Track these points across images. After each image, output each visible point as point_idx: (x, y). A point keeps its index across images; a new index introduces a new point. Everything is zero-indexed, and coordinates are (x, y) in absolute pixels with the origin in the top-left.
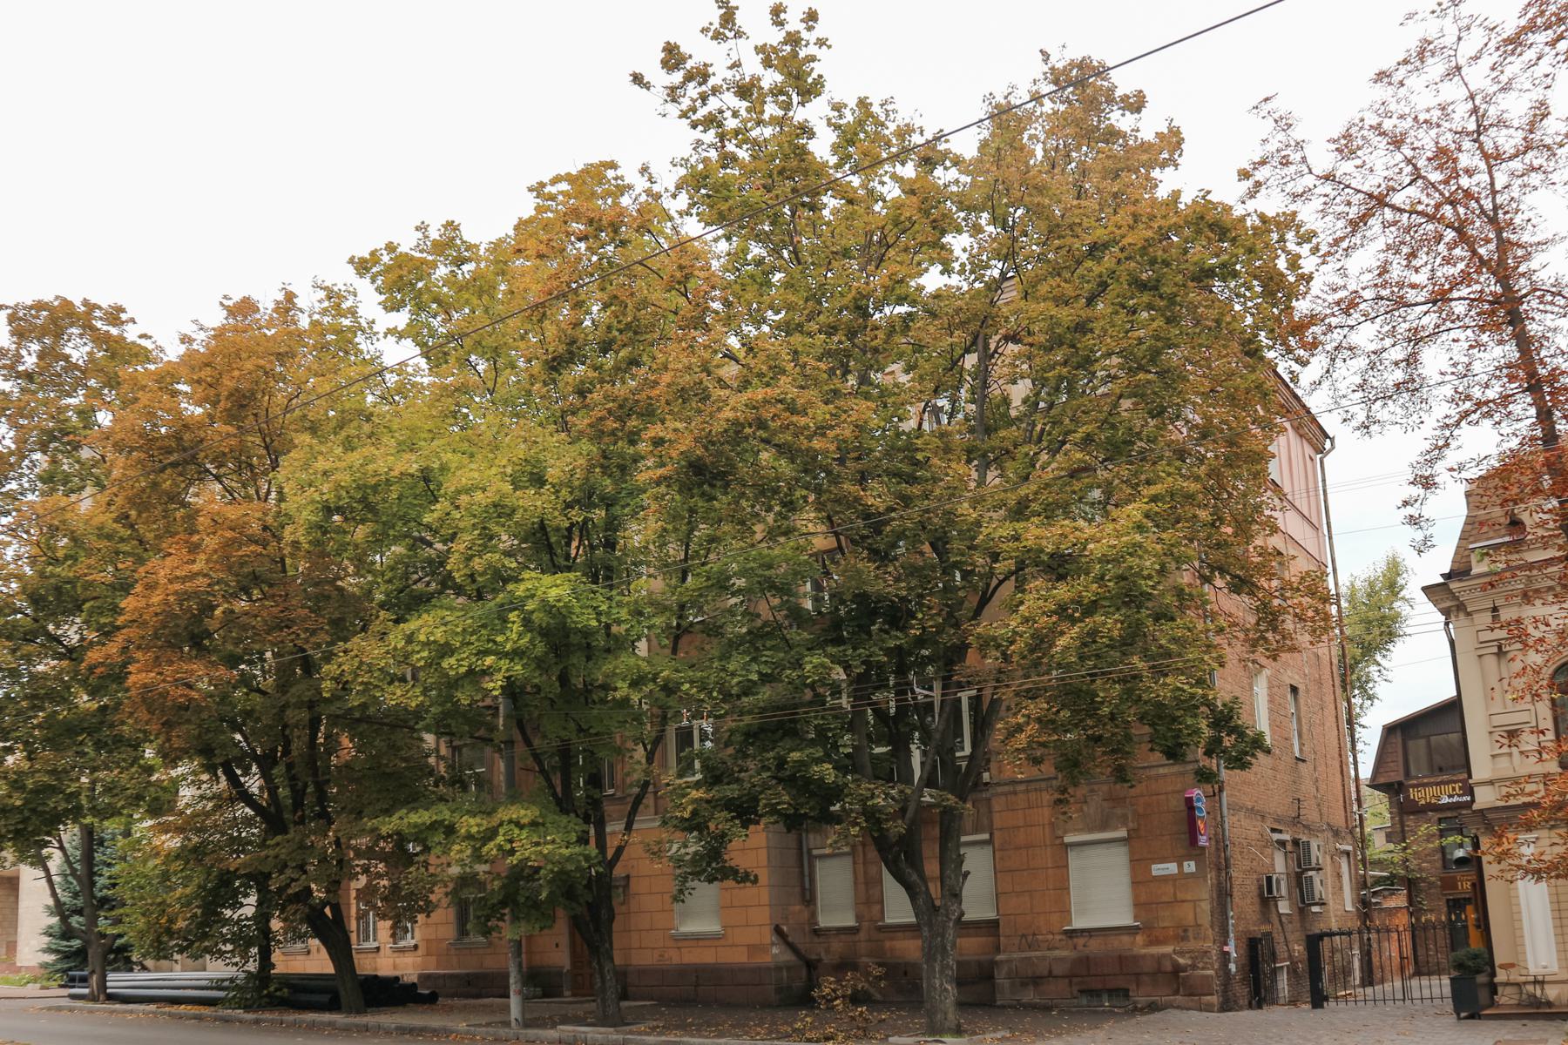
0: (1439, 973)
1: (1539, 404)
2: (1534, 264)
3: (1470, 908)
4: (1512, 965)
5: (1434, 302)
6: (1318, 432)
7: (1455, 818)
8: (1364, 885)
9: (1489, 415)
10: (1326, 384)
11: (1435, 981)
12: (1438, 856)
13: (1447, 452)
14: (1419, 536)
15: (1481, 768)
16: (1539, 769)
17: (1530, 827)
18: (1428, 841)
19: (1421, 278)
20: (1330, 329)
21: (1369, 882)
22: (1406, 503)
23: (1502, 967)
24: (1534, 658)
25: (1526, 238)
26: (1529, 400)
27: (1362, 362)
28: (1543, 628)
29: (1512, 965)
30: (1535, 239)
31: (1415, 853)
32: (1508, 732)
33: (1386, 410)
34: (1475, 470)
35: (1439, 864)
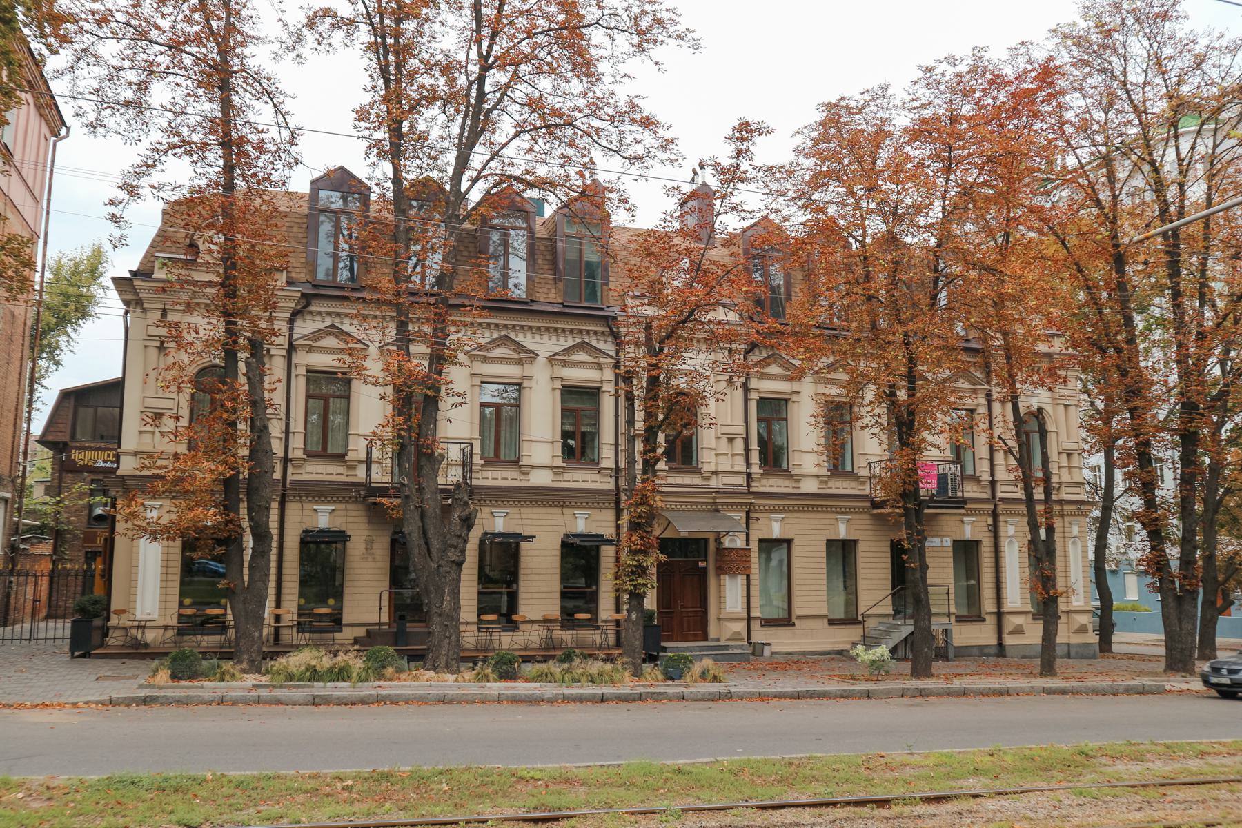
0: (64, 617)
1: (227, 157)
2: (247, 51)
3: (99, 559)
4: (124, 612)
5: (171, 48)
6: (57, 118)
7: (105, 481)
8: (16, 533)
9: (189, 153)
10: (67, 77)
11: (60, 624)
12: (85, 512)
13: (152, 171)
14: (118, 233)
15: (130, 439)
16: (171, 448)
17: (155, 495)
18: (79, 498)
19: (165, 24)
20: (81, 31)
21: (21, 528)
22: (112, 203)
23: (116, 612)
24: (185, 358)
25: (246, 29)
26: (220, 152)
27: (103, 72)
28: (193, 334)
29: (124, 612)
30: (252, 33)
31: (67, 507)
32: (155, 414)
33: (113, 119)
34: (170, 193)
35: (85, 520)
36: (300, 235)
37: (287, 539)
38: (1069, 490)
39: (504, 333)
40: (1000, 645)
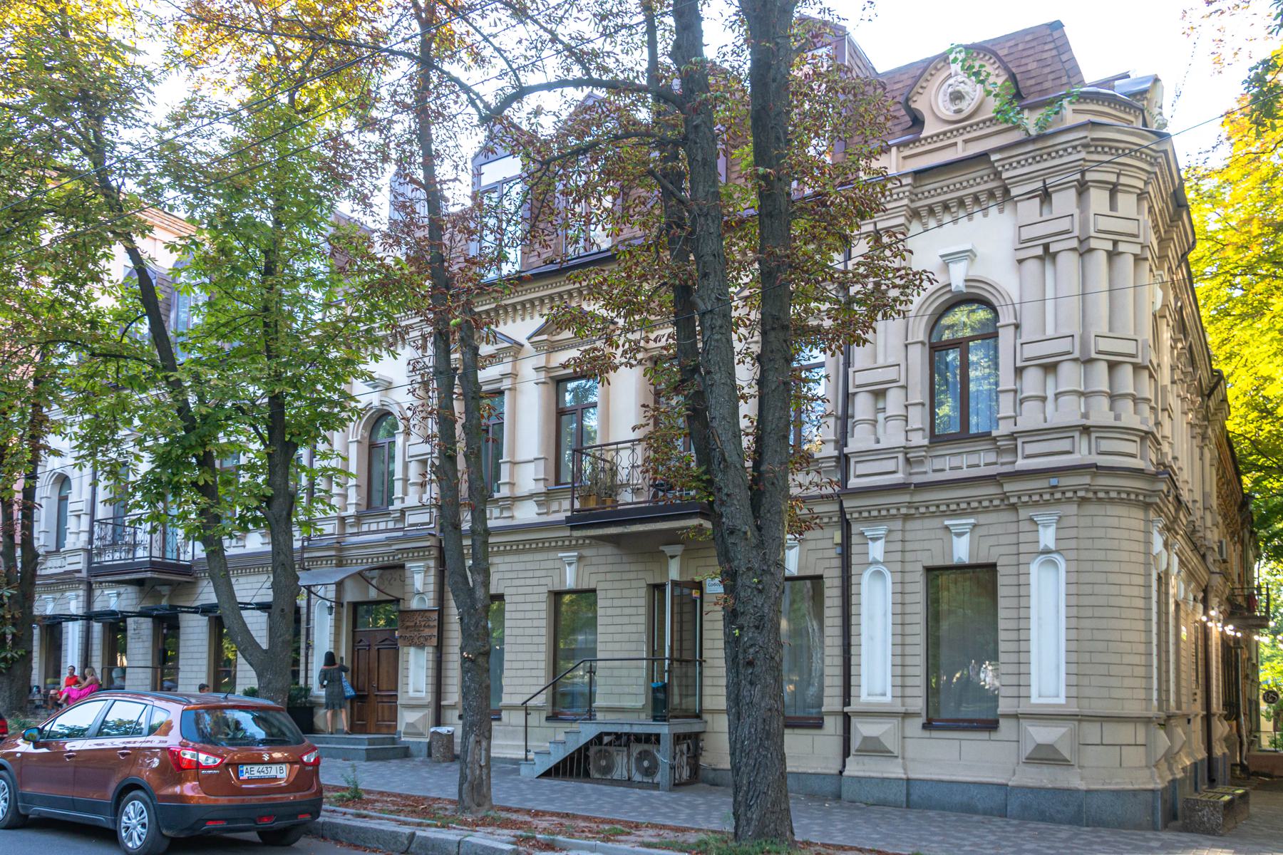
38: (1030, 449)
40: (841, 773)
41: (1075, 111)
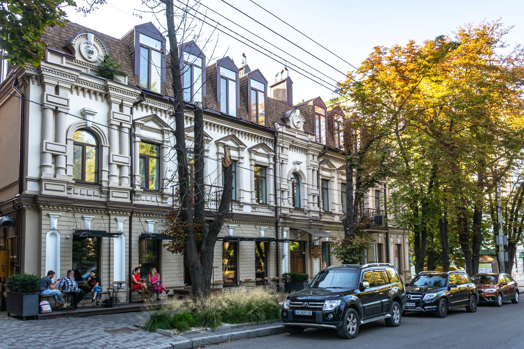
36: (127, 58)
37: (133, 239)
39: (154, 113)
41: (67, 63)
